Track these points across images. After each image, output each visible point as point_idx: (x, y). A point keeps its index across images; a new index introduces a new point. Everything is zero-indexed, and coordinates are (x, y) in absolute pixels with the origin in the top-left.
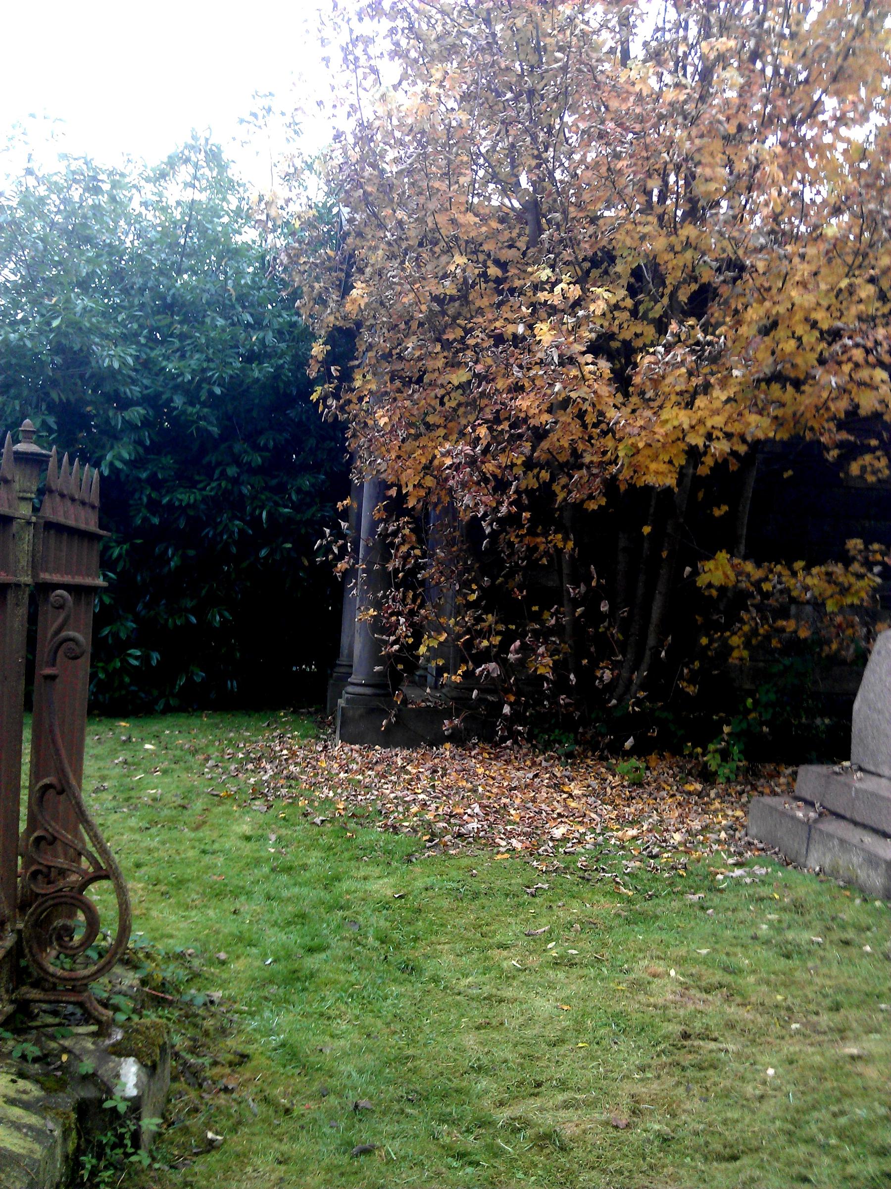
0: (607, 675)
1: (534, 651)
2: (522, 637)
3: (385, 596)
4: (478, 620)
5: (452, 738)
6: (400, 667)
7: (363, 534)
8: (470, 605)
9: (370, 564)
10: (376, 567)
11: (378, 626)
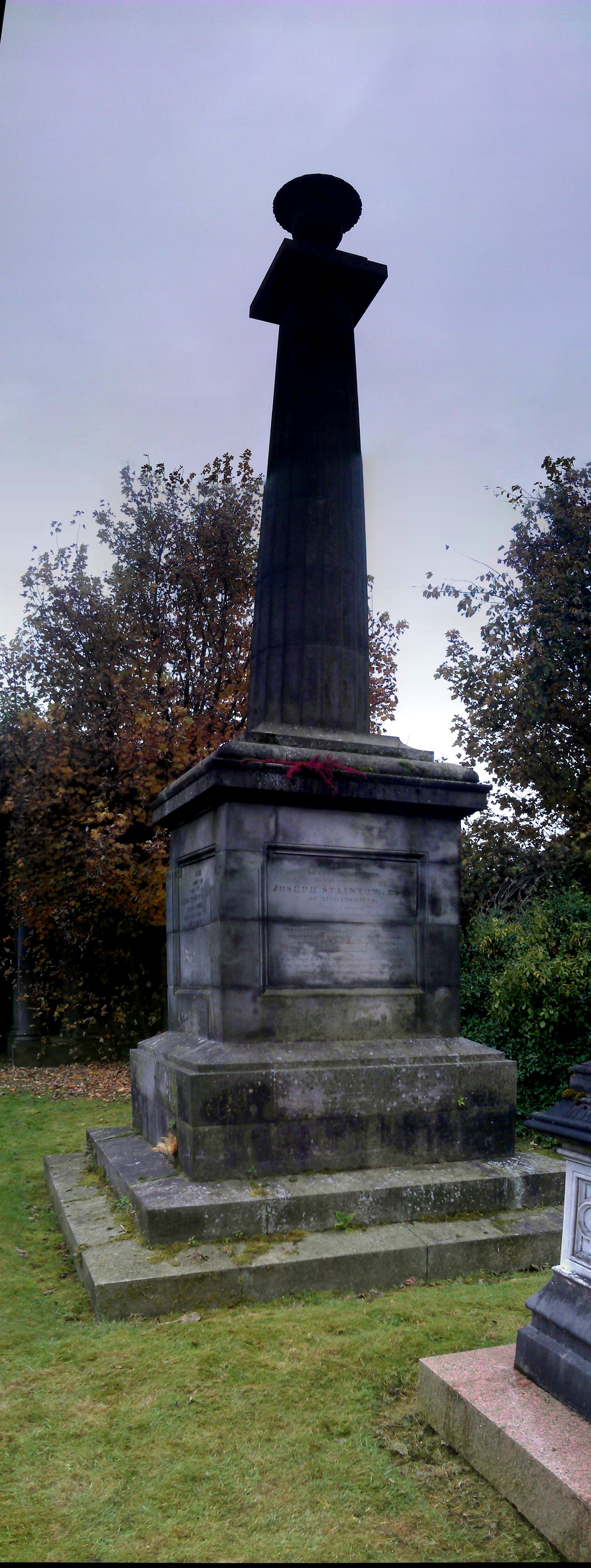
0: (154, 1019)
1: (115, 1010)
2: (108, 1003)
3: (34, 987)
4: (86, 996)
5: (77, 1061)
6: (44, 1024)
7: (19, 955)
8: (80, 988)
9: (24, 970)
10: (27, 971)
11: (32, 1003)
